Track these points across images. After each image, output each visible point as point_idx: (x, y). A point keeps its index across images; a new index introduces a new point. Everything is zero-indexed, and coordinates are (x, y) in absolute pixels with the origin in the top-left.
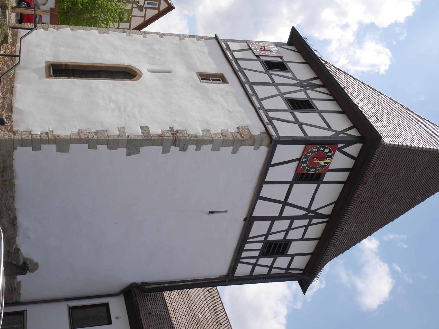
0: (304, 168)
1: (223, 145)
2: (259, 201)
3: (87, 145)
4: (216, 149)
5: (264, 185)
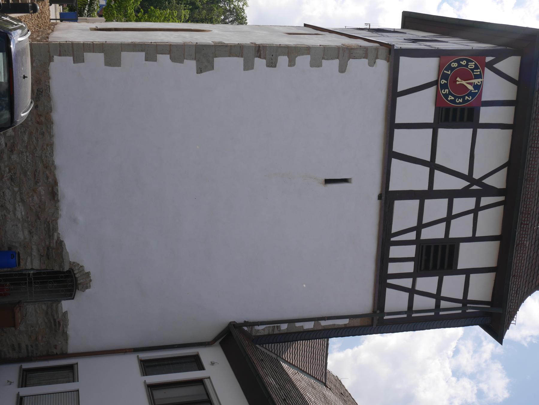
0: (446, 96)
1: (326, 57)
2: (397, 132)
3: (143, 54)
4: (316, 63)
5: (399, 99)
